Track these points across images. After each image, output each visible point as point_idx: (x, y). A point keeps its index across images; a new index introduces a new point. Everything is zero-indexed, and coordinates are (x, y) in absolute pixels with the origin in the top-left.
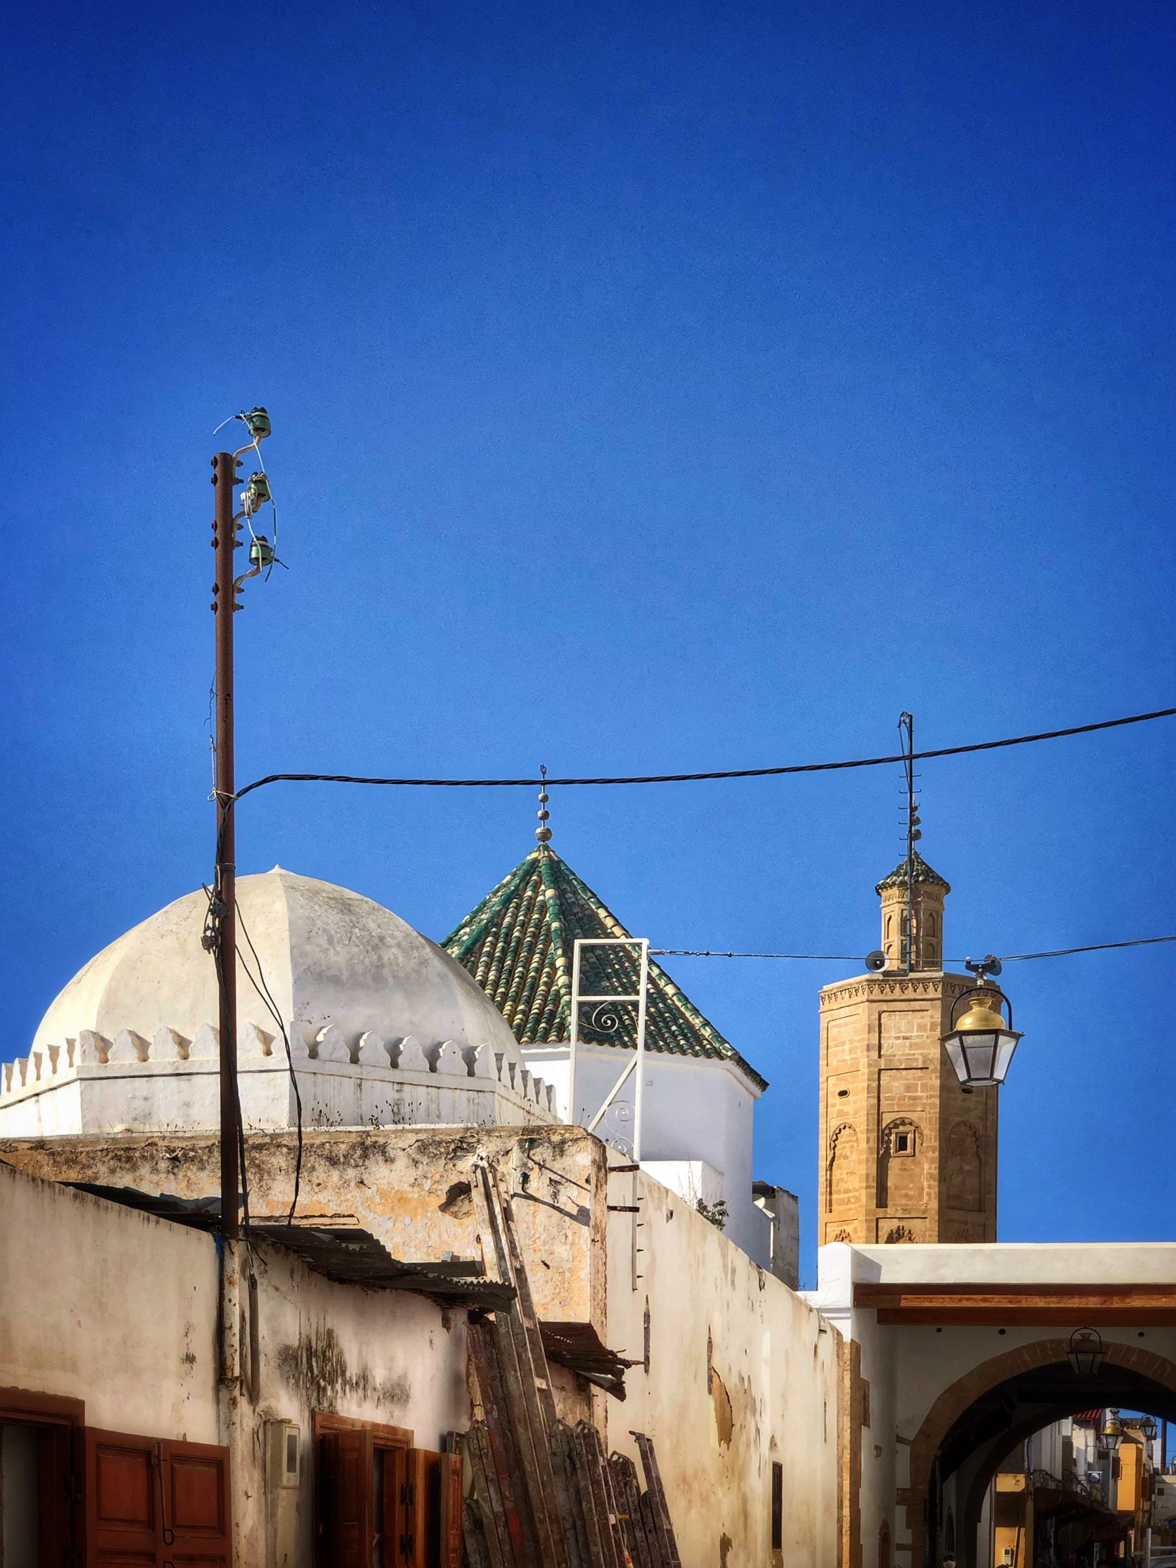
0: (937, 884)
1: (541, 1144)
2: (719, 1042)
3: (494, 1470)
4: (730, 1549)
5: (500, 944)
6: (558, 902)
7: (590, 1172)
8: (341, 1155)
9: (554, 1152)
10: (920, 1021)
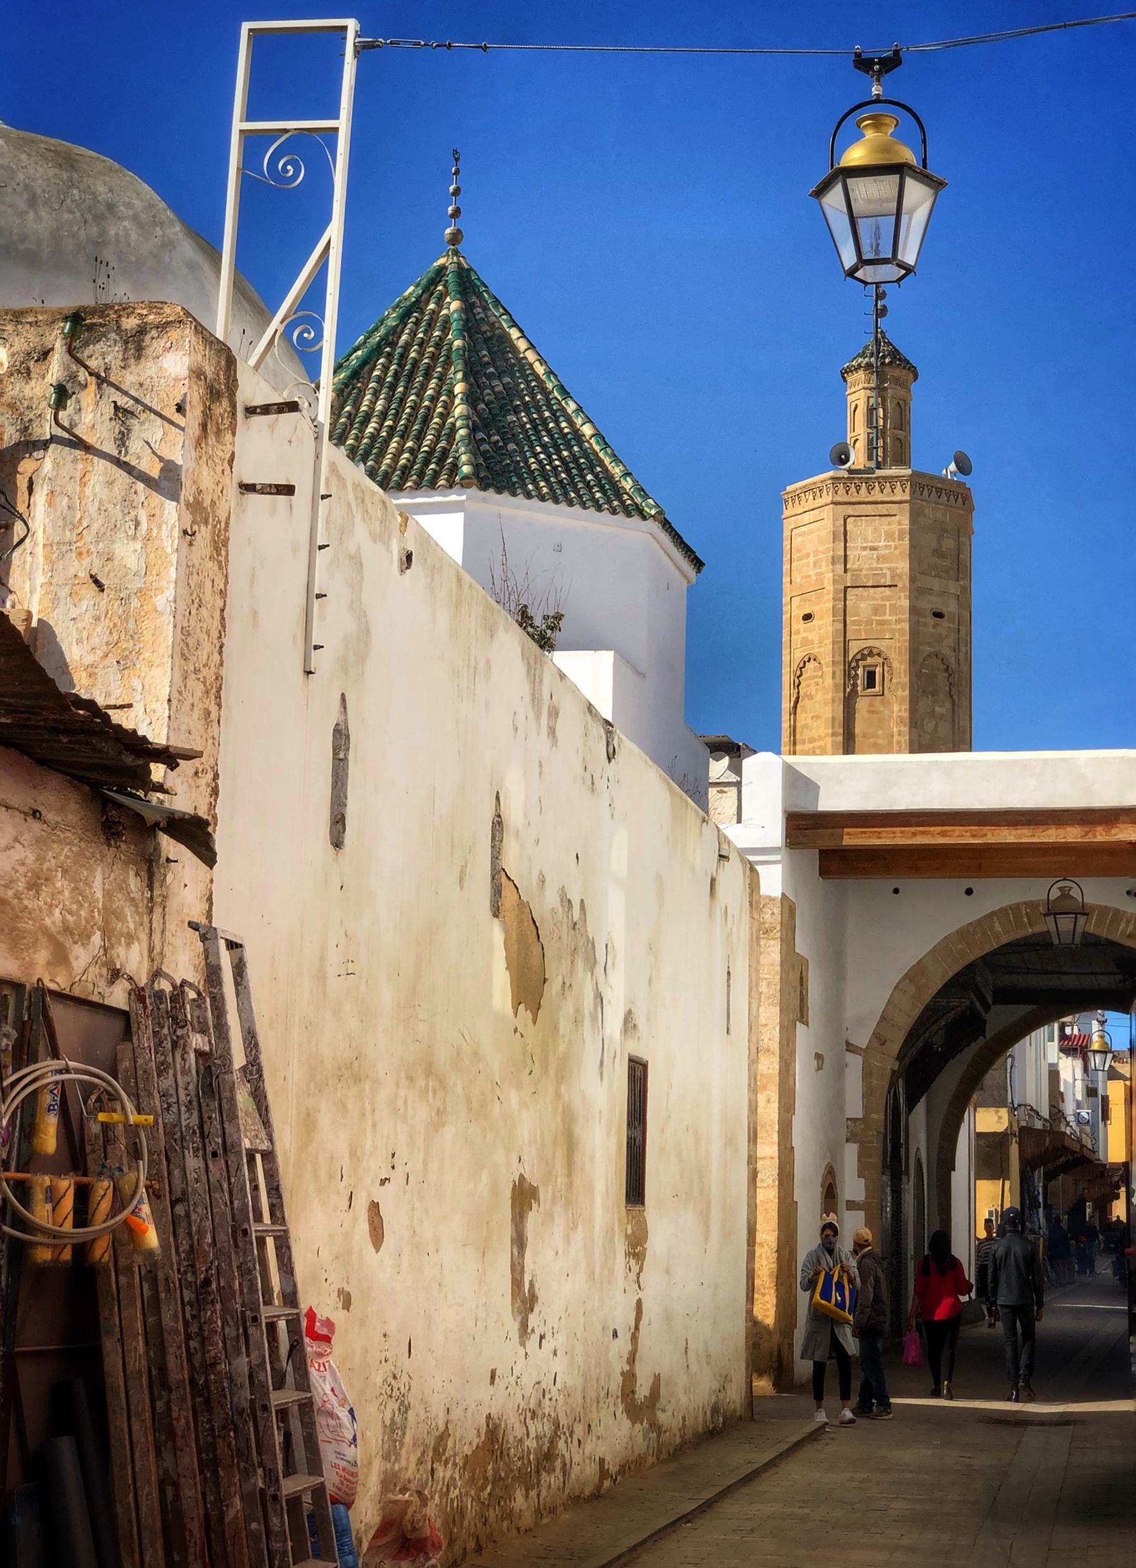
0: (904, 368)
1: (104, 335)
2: (641, 496)
4: (535, 1206)
5: (393, 367)
6: (463, 315)
7: (184, 390)
9: (126, 350)
10: (886, 528)
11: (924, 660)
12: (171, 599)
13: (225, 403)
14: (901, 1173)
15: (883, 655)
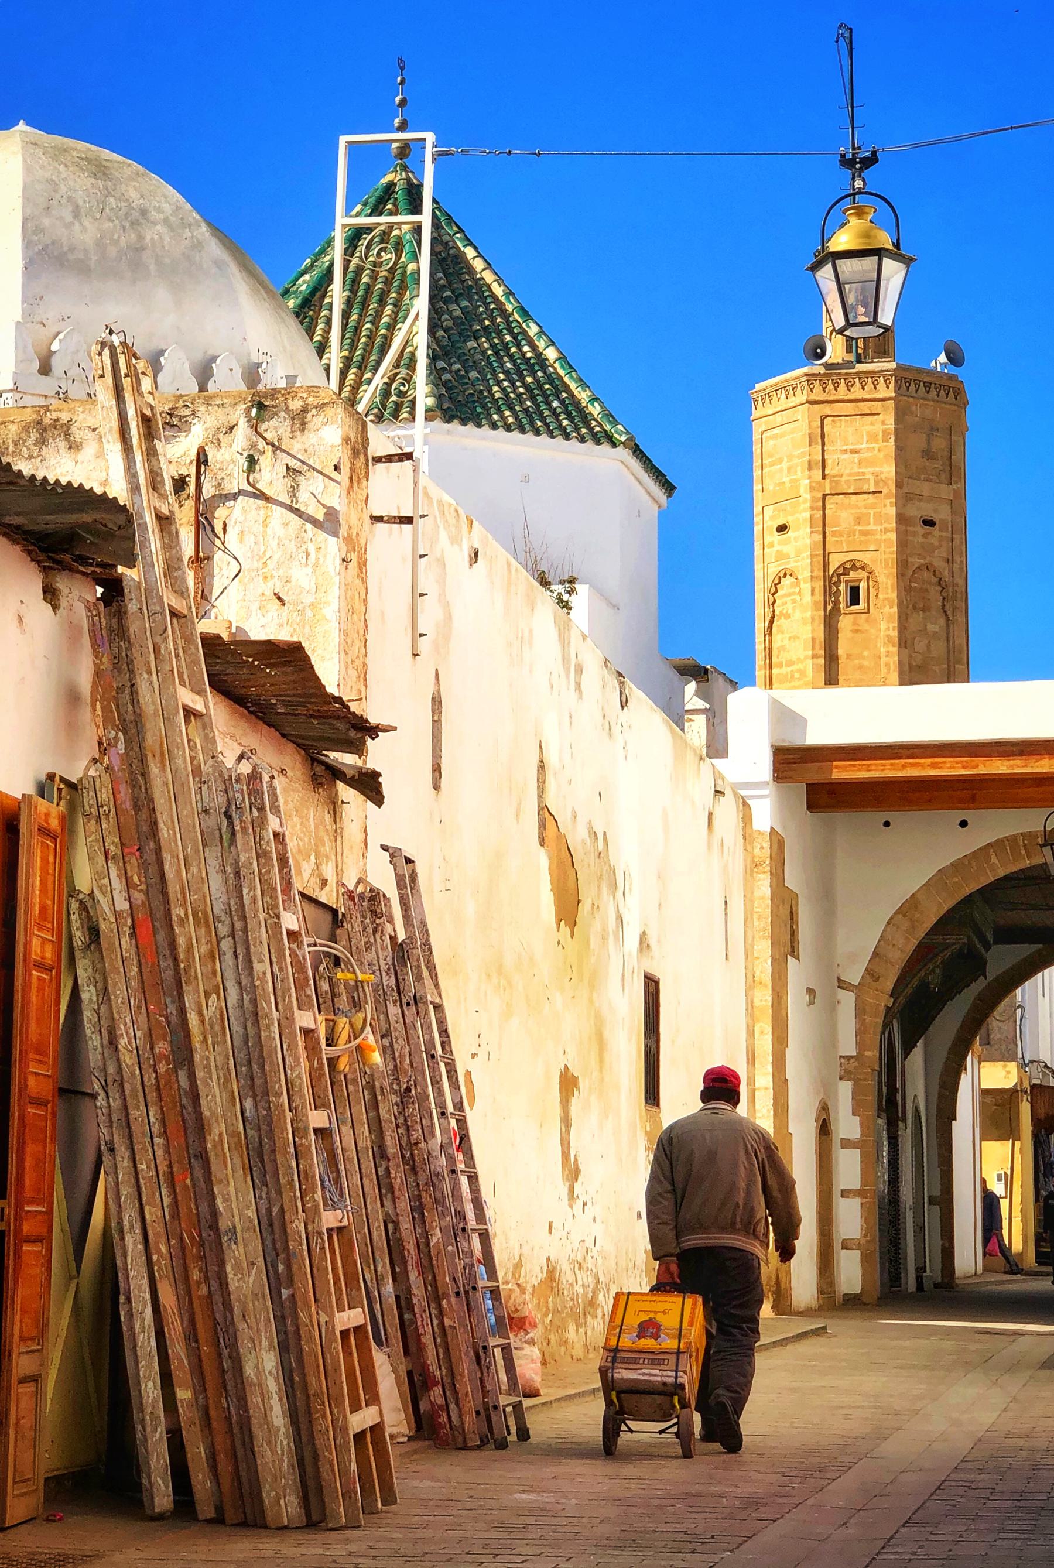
1: (276, 414)
2: (610, 422)
3: (117, 840)
4: (576, 1093)
7: (339, 454)
8: (10, 441)
9: (293, 425)
10: (869, 428)
11: (914, 572)
12: (337, 609)
13: (362, 457)
14: (897, 1119)
15: (868, 569)
